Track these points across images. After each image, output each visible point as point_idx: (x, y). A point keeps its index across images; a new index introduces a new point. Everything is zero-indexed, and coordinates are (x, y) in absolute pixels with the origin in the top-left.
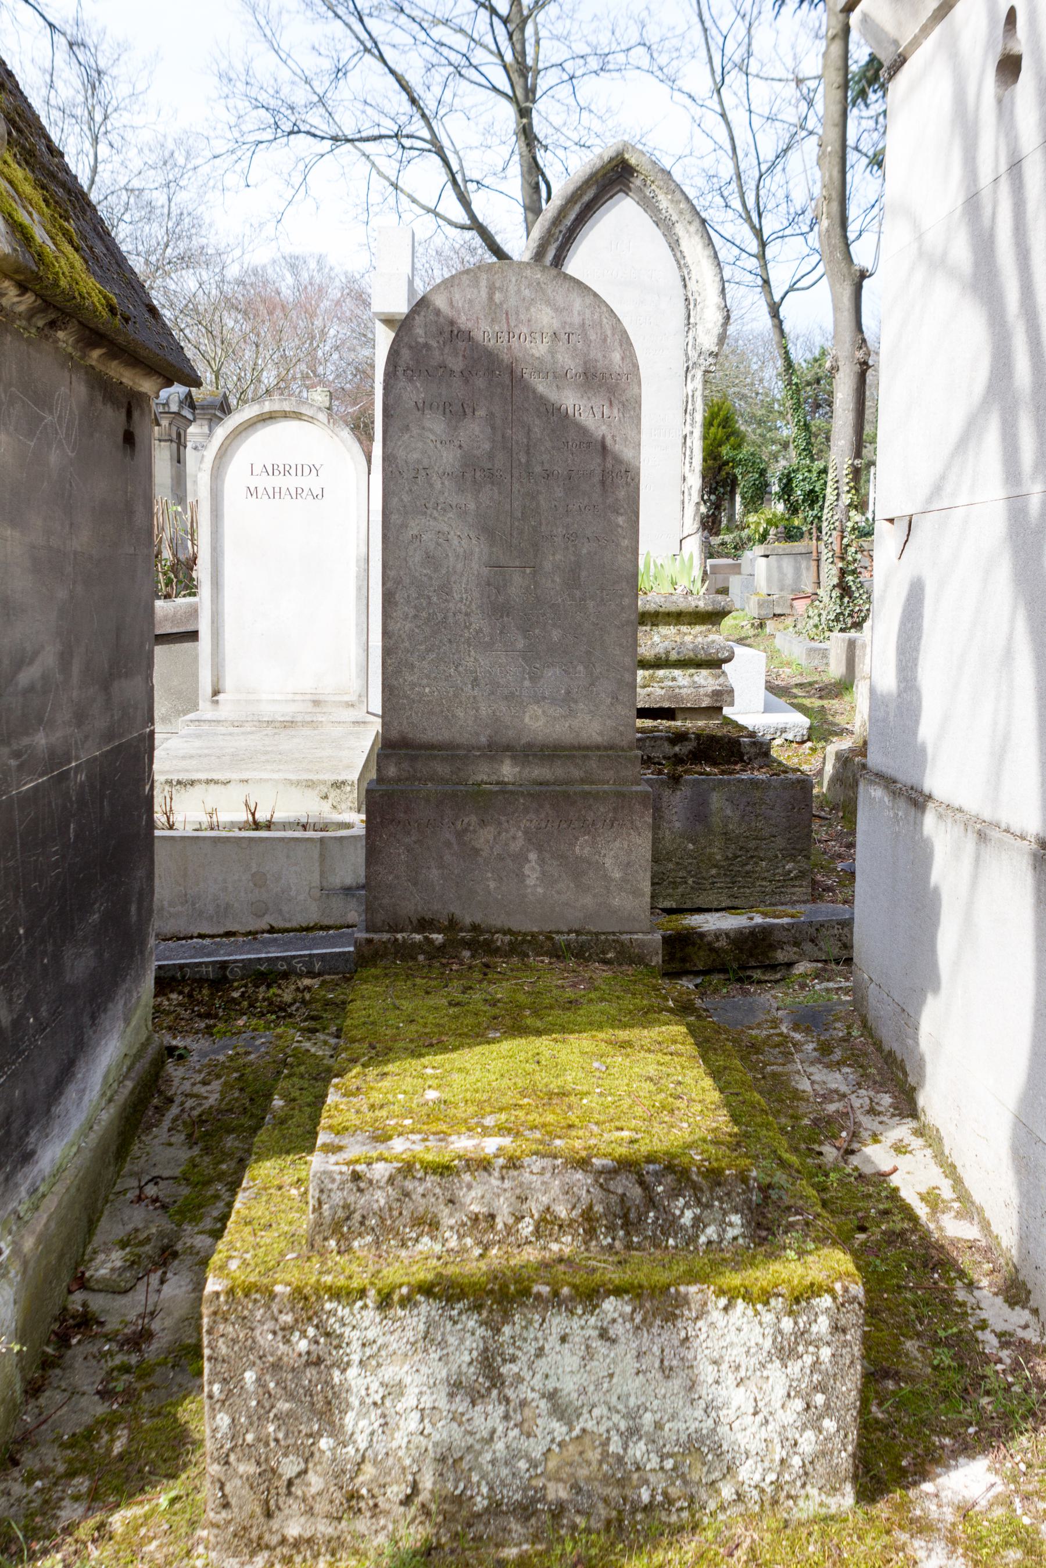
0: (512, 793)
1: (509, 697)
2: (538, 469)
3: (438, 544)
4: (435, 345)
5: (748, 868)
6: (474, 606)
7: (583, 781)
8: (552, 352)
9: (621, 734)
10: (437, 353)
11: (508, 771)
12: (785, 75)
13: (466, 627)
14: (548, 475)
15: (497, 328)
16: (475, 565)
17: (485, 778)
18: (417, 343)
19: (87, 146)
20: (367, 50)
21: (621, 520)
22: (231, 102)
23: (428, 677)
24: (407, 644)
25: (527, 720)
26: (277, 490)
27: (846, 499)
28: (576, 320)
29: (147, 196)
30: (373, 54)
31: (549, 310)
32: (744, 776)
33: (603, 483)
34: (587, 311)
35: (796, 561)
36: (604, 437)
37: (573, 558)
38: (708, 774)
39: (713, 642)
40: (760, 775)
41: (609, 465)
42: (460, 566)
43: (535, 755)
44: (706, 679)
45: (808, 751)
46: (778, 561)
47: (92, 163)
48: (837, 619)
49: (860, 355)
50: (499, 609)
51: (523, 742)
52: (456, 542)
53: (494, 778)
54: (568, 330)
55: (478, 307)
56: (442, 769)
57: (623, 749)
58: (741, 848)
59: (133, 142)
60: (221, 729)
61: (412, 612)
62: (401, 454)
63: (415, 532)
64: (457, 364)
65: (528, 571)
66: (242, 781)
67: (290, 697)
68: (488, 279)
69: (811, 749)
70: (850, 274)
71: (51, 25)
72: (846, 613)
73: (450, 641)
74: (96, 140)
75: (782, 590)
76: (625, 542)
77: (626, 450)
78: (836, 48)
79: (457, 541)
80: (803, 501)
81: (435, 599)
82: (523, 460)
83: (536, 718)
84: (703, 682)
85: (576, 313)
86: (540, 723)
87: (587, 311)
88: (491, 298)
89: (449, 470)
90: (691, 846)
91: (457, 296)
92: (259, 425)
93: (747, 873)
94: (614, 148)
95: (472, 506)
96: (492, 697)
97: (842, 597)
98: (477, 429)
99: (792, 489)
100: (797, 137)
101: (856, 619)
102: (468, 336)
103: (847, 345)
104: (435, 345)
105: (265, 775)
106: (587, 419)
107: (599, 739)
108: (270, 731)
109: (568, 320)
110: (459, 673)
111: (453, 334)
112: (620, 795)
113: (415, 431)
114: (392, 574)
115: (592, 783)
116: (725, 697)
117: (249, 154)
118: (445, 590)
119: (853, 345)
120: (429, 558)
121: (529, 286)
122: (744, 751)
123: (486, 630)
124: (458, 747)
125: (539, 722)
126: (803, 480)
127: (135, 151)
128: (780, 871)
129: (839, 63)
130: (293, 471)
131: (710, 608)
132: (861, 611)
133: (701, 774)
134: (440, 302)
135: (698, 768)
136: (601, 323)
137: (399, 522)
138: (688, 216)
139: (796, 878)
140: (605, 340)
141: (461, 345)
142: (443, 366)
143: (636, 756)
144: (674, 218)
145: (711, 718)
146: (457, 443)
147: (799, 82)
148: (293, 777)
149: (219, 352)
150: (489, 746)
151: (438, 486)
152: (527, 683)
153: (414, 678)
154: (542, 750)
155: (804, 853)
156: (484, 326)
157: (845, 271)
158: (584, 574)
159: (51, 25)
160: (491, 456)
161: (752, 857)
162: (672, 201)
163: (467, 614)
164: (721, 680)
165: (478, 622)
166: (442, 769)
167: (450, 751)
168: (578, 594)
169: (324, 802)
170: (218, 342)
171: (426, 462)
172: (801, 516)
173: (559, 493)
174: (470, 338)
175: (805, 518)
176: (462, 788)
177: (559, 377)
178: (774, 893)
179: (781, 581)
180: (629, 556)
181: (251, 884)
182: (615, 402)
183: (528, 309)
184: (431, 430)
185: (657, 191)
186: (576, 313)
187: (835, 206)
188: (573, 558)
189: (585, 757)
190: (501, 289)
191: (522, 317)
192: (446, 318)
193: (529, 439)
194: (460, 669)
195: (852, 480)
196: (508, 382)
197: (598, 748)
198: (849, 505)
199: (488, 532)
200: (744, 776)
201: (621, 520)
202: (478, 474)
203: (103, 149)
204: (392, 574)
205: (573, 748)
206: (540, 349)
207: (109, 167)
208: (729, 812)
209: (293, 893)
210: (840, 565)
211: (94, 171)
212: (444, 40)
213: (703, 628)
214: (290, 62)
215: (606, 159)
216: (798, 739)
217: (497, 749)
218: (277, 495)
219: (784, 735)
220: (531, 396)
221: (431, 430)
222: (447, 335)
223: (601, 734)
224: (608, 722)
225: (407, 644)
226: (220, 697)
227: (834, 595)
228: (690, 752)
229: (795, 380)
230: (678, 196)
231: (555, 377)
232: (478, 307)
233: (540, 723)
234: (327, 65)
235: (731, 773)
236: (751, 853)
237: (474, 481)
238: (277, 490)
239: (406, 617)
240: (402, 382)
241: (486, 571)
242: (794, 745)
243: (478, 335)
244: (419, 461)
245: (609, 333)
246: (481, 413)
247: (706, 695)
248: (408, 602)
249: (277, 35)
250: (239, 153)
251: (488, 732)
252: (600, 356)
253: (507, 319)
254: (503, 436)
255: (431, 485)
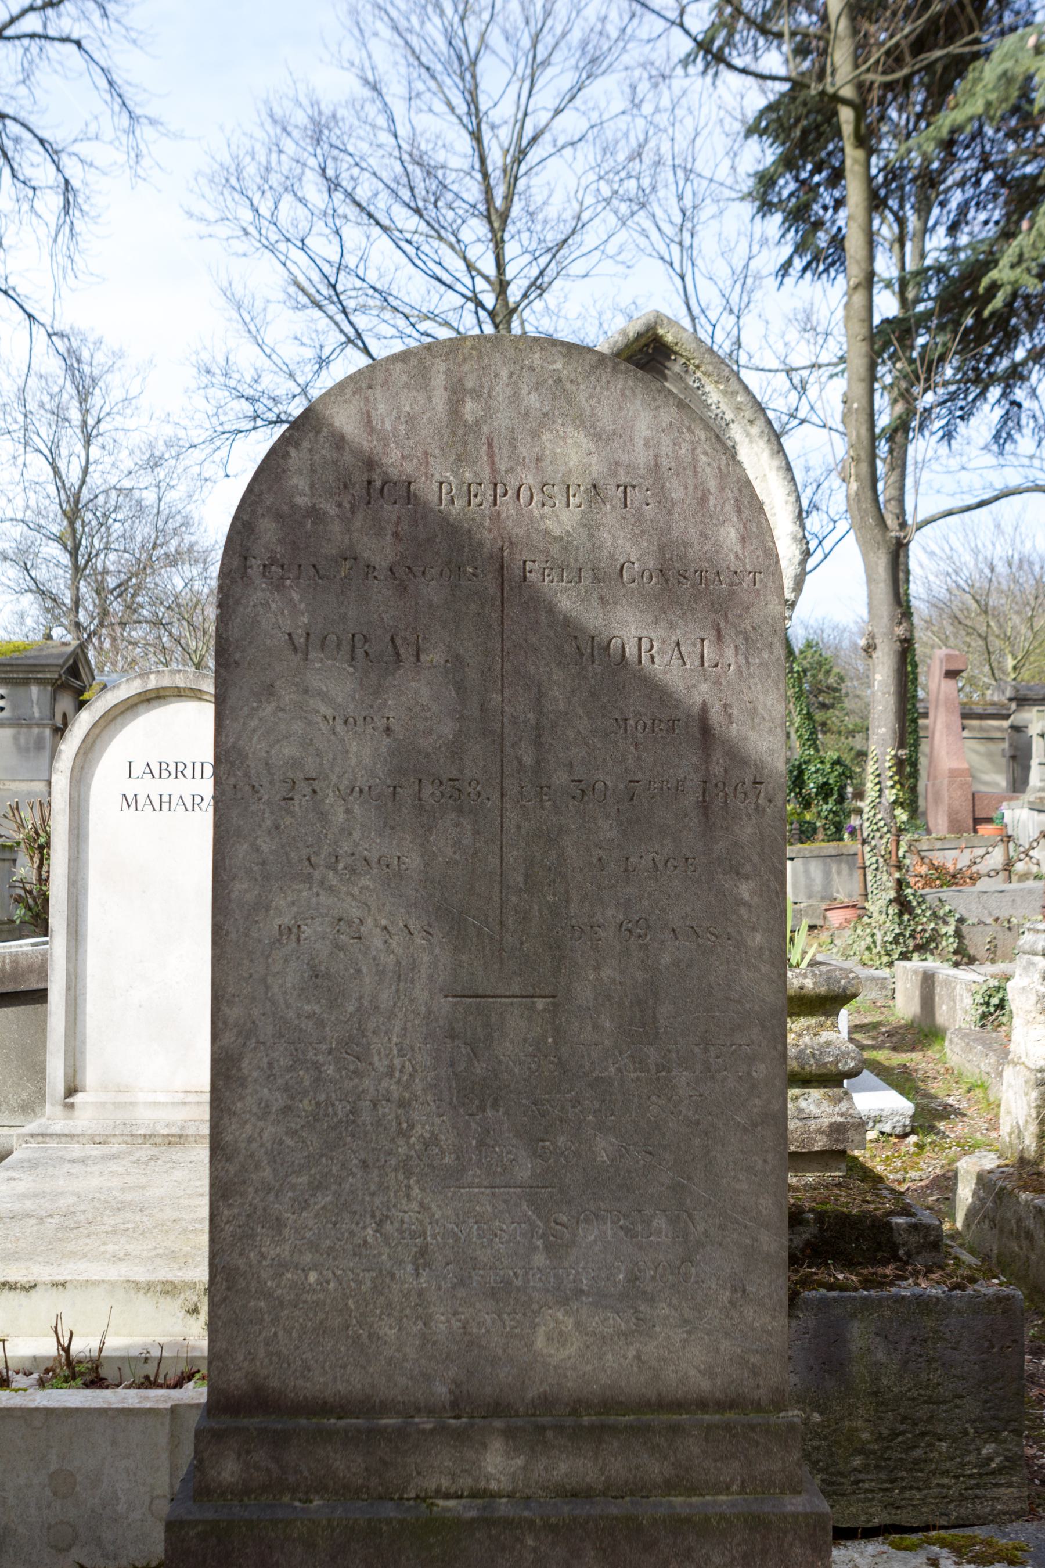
0: (507, 1523)
1: (501, 1292)
2: (560, 779)
3: (339, 947)
4: (333, 511)
5: (917, 1453)
6: (418, 1086)
7: (670, 1487)
8: (590, 526)
9: (755, 1372)
10: (336, 527)
11: (498, 1465)
12: (775, 364)
13: (401, 1132)
14: (583, 791)
15: (468, 475)
16: (420, 994)
17: (445, 1483)
18: (293, 506)
19: (79, 448)
20: (350, 341)
21: (745, 890)
22: (211, 392)
23: (314, 1246)
24: (267, 1173)
25: (540, 1343)
26: (165, 799)
27: (890, 795)
28: (642, 457)
29: (137, 494)
30: (356, 345)
31: (581, 438)
32: (905, 1289)
33: (705, 807)
34: (666, 440)
35: (825, 864)
36: (704, 709)
37: (640, 976)
38: (843, 1288)
39: (829, 1044)
40: (930, 1288)
41: (717, 770)
42: (386, 996)
43: (559, 1429)
44: (818, 1105)
45: (912, 1149)
46: (804, 864)
47: (83, 463)
48: (896, 941)
49: (900, 631)
50: (473, 1092)
51: (531, 1394)
52: (377, 942)
53: (466, 1482)
54: (624, 480)
55: (426, 432)
56: (347, 1464)
57: (758, 1407)
58: (904, 1419)
59: (125, 444)
60: (75, 1150)
61: (279, 1100)
62: (256, 747)
63: (287, 920)
64: (380, 551)
65: (540, 1004)
66: (55, 1284)
67: (180, 1097)
68: (448, 372)
69: (916, 1145)
70: (885, 541)
71: (30, 316)
72: (907, 934)
73: (365, 1165)
74: (88, 443)
75: (810, 897)
76: (758, 939)
77: (753, 736)
78: (859, 298)
79: (386, 945)
80: (817, 794)
81: (330, 1070)
82: (528, 760)
83: (560, 1338)
84: (813, 1109)
85: (640, 443)
86: (572, 1350)
87: (666, 440)
88: (455, 410)
89: (361, 782)
90: (816, 1417)
91: (382, 408)
92: (141, 708)
93: (916, 1462)
94: (641, 322)
95: (414, 861)
96: (461, 1292)
97: (900, 914)
98: (425, 691)
99: (803, 782)
100: (789, 426)
101: (919, 941)
102: (405, 492)
103: (885, 620)
104: (333, 511)
105: (95, 1271)
106: (667, 668)
107: (705, 1385)
108: (144, 1152)
109: (624, 458)
110: (386, 1238)
111: (372, 487)
112: (757, 1523)
113: (287, 696)
114: (234, 1013)
115: (692, 1490)
116: (851, 1134)
117: (229, 442)
118: (354, 1048)
119: (892, 618)
120: (317, 977)
121: (537, 387)
122: (899, 1240)
123: (448, 1139)
124: (385, 1408)
125: (567, 1347)
126: (816, 772)
127: (127, 452)
128: (972, 1458)
129: (864, 314)
130: (188, 772)
131: (823, 990)
132: (924, 930)
133: (831, 1287)
134: (345, 419)
135: (822, 1275)
136: (694, 464)
137: (250, 897)
138: (749, 414)
139: (1000, 1470)
140: (703, 500)
141: (390, 511)
142: (350, 556)
143: (791, 1427)
144: (729, 416)
145: (827, 1168)
146: (380, 723)
147: (789, 371)
148: (141, 1274)
149: (200, 644)
150: (455, 1404)
151: (339, 817)
152: (539, 1259)
153: (284, 1251)
154: (574, 1412)
155: (1014, 1425)
156: (441, 470)
157: (879, 537)
158: (665, 1010)
159: (30, 316)
160: (456, 750)
161: (923, 1434)
162: (725, 393)
163: (403, 1104)
164: (843, 1106)
165: (428, 1120)
166: (347, 1464)
167: (364, 1421)
168: (652, 1053)
169: (191, 1320)
170: (200, 634)
171: (311, 766)
172: (814, 810)
173: (608, 830)
174: (410, 497)
175: (819, 813)
176: (389, 1511)
177: (606, 579)
178: (963, 1498)
179: (809, 887)
180: (765, 968)
181: (48, 1493)
182: (729, 632)
183: (535, 435)
184: (322, 695)
185: (704, 380)
186: (640, 443)
187: (864, 467)
188: (640, 976)
189: (675, 1429)
190: (476, 393)
191: (523, 451)
192: (358, 453)
193: (540, 712)
194: (388, 1227)
195: (896, 773)
196: (493, 590)
197: (702, 1404)
198: (895, 802)
199: (449, 913)
200: (905, 1289)
201: (745, 890)
202: (427, 790)
203: (94, 451)
204: (234, 1013)
205: (644, 1405)
206: (563, 519)
207: (100, 467)
208: (880, 1356)
209: (121, 1508)
210: (897, 875)
211: (85, 471)
212: (429, 331)
213: (812, 1021)
214: (274, 356)
215: (632, 334)
216: (898, 1131)
217: (478, 1411)
218: (165, 806)
219: (879, 1126)
220: (544, 619)
221: (322, 695)
222: (359, 490)
223: (709, 1373)
224: (725, 1345)
225: (267, 1173)
226: (78, 1098)
227: (891, 911)
228: (808, 1244)
229: (796, 668)
230: (734, 385)
231: (597, 579)
232: (426, 432)
233: (572, 1350)
234: (310, 353)
235: (881, 1285)
236: (920, 1428)
237: (420, 807)
238: (165, 799)
239: (265, 1113)
240: (259, 592)
241: (444, 1005)
242: (893, 1140)
243: (427, 489)
244: (296, 764)
245: (712, 485)
246: (435, 656)
247: (820, 1131)
248: (270, 1077)
249: (262, 331)
250: (218, 443)
251: (453, 1371)
252: (693, 533)
253: (491, 456)
254: (483, 708)
255: (323, 816)
